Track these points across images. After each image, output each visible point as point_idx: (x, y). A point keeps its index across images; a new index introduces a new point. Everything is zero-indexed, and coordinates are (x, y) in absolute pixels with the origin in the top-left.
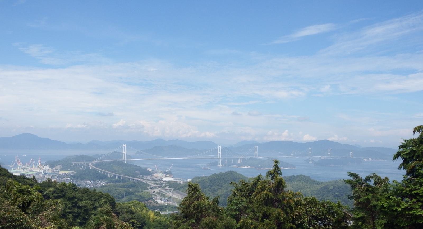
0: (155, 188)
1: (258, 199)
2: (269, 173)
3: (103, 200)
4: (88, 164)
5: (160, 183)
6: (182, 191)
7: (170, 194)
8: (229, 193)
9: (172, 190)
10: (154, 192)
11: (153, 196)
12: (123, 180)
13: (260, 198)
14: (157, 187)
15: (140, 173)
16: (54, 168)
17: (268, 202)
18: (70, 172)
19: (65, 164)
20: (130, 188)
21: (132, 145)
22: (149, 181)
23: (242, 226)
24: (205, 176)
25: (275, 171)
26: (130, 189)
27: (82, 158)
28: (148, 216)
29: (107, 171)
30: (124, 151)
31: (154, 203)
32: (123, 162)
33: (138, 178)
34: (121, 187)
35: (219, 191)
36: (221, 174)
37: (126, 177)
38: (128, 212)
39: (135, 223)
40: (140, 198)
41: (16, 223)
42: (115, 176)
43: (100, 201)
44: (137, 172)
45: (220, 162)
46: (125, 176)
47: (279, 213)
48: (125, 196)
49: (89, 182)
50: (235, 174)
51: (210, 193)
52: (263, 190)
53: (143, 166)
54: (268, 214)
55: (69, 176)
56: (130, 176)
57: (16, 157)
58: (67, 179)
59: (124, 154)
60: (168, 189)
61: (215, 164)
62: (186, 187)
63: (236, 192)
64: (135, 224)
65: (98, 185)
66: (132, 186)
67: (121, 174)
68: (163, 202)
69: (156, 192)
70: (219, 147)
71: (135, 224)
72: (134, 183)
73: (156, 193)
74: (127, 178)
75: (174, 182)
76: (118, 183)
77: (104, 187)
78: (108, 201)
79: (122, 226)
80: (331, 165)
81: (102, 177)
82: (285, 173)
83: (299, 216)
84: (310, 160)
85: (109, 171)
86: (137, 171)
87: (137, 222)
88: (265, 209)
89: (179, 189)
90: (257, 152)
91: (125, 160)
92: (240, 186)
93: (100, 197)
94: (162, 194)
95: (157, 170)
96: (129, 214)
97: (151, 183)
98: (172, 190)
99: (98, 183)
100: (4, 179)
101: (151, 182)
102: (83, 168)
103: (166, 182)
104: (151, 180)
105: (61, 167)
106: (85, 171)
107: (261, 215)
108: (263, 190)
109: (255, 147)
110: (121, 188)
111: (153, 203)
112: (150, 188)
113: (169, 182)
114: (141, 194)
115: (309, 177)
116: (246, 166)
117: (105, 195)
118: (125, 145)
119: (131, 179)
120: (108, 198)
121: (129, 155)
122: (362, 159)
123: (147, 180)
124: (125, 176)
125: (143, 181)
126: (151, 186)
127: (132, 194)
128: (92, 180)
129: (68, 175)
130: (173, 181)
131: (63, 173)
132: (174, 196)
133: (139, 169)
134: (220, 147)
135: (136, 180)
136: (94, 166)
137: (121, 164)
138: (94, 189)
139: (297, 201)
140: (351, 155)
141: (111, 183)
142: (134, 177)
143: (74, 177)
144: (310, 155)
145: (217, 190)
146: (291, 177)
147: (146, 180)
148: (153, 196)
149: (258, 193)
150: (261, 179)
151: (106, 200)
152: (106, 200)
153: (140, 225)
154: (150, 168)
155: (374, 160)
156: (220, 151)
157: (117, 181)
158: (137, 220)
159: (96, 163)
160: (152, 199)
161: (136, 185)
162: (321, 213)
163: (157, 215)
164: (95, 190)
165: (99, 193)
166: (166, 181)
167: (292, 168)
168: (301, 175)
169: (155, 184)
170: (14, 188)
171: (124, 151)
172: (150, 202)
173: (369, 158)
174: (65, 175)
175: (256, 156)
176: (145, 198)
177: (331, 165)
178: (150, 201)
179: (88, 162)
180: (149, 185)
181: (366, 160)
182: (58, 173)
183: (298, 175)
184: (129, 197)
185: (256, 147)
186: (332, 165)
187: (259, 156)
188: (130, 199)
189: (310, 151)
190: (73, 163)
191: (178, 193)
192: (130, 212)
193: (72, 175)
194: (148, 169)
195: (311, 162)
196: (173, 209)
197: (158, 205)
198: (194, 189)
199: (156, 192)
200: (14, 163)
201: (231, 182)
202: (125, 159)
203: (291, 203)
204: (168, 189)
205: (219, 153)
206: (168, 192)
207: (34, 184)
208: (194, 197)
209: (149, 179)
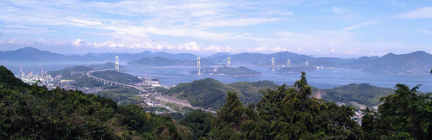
0: (145, 93)
1: (288, 105)
2: (297, 83)
3: (107, 104)
4: (86, 73)
5: (150, 90)
6: (169, 95)
7: (158, 98)
8: (208, 97)
9: (160, 94)
10: (144, 96)
11: (144, 100)
12: (117, 87)
13: (290, 104)
14: (147, 92)
15: (131, 80)
16: (55, 77)
17: (297, 107)
18: (70, 81)
19: (66, 73)
20: (123, 93)
21: (124, 56)
22: (140, 87)
23: (274, 127)
24: (188, 82)
25: (301, 81)
26: (123, 94)
27: (81, 68)
28: (145, 117)
29: (103, 79)
30: (117, 62)
31: (145, 105)
32: (117, 71)
33: (130, 84)
34: (115, 93)
35: (200, 95)
36: (201, 81)
37: (120, 84)
38: (128, 114)
39: (135, 123)
40: (133, 101)
41: (101, 131)
42: (110, 83)
43: (104, 105)
44: (129, 79)
45: (200, 71)
46: (119, 83)
47: (309, 116)
48: (120, 100)
49: (87, 88)
50: (212, 80)
51: (192, 96)
52: (293, 96)
53: (133, 74)
54: (297, 117)
55: (70, 84)
56: (123, 83)
57: (21, 68)
58: (68, 86)
59: (117, 64)
60: (157, 93)
61: (195, 72)
62: (171, 91)
63: (266, 99)
64: (135, 124)
65: (96, 91)
66: (125, 92)
67: (115, 82)
68: (153, 104)
69: (146, 96)
70: (198, 58)
71: (135, 124)
72: (127, 89)
73: (146, 97)
74: (121, 85)
75: (162, 88)
76: (113, 89)
77: (101, 93)
78: (111, 105)
79: (181, 129)
80: (290, 72)
81: (99, 85)
82: (310, 81)
83: (325, 118)
84: (273, 68)
85: (104, 79)
86: (128, 79)
87: (136, 122)
88: (295, 113)
89: (166, 94)
90: (229, 62)
91: (118, 70)
92: (267, 94)
93: (104, 102)
94: (151, 97)
95: (146, 78)
96: (129, 116)
97: (142, 89)
98: (160, 94)
99: (95, 89)
100: (19, 88)
101: (142, 88)
102: (82, 77)
103: (154, 88)
104: (141, 87)
105: (62, 76)
106: (84, 79)
107: (292, 118)
108: (293, 96)
109: (228, 58)
110: (116, 93)
111: (144, 105)
112: (141, 93)
113: (157, 88)
114: (133, 98)
115: (273, 82)
116: (220, 74)
117: (108, 100)
118: (118, 57)
119: (124, 85)
120: (111, 103)
121: (121, 66)
122: (316, 67)
123: (138, 86)
124: (119, 83)
125: (135, 87)
126: (142, 91)
127: (125, 98)
128: (90, 87)
129: (68, 83)
130: (161, 87)
131: (64, 81)
132: (162, 99)
133: (131, 77)
134: (199, 58)
135: (128, 86)
136: (91, 75)
137: (115, 73)
138: (98, 94)
139: (321, 106)
140: (307, 63)
141: (107, 89)
142: (126, 84)
143: (74, 84)
144: (273, 64)
145: (198, 94)
146: (258, 82)
147: (138, 87)
148: (144, 100)
149: (288, 100)
150: (285, 87)
151: (109, 104)
152: (109, 104)
153: (139, 124)
154: (140, 76)
155: (325, 68)
156: (199, 62)
157: (112, 88)
158: (137, 120)
159: (93, 72)
160: (143, 102)
161: (129, 91)
162: (342, 115)
163: (153, 115)
164: (99, 96)
165: (102, 99)
166: (155, 87)
167: (258, 75)
168: (266, 81)
169: (145, 89)
170: (75, 99)
171: (117, 62)
172: (141, 105)
173: (321, 66)
174: (65, 83)
175: (229, 65)
176: (137, 101)
177: (290, 72)
178: (142, 104)
179: (85, 72)
180: (140, 91)
181: (319, 68)
182: (59, 82)
183: (264, 81)
184: (123, 101)
185: (273, 59)
186: (291, 72)
187: (231, 65)
188: (124, 102)
189: (273, 61)
190: (72, 73)
191: (166, 97)
192: (130, 114)
193: (72, 83)
194: (138, 77)
195: (274, 70)
196: (162, 110)
197: (148, 107)
198: (234, 97)
199: (146, 96)
200: (19, 74)
201: (260, 91)
202: (118, 69)
203: (318, 107)
204: (157, 93)
205: (199, 64)
206: (157, 96)
207: (46, 91)
208: (233, 104)
209: (139, 85)
